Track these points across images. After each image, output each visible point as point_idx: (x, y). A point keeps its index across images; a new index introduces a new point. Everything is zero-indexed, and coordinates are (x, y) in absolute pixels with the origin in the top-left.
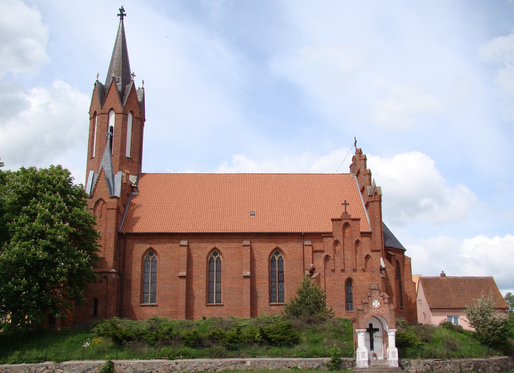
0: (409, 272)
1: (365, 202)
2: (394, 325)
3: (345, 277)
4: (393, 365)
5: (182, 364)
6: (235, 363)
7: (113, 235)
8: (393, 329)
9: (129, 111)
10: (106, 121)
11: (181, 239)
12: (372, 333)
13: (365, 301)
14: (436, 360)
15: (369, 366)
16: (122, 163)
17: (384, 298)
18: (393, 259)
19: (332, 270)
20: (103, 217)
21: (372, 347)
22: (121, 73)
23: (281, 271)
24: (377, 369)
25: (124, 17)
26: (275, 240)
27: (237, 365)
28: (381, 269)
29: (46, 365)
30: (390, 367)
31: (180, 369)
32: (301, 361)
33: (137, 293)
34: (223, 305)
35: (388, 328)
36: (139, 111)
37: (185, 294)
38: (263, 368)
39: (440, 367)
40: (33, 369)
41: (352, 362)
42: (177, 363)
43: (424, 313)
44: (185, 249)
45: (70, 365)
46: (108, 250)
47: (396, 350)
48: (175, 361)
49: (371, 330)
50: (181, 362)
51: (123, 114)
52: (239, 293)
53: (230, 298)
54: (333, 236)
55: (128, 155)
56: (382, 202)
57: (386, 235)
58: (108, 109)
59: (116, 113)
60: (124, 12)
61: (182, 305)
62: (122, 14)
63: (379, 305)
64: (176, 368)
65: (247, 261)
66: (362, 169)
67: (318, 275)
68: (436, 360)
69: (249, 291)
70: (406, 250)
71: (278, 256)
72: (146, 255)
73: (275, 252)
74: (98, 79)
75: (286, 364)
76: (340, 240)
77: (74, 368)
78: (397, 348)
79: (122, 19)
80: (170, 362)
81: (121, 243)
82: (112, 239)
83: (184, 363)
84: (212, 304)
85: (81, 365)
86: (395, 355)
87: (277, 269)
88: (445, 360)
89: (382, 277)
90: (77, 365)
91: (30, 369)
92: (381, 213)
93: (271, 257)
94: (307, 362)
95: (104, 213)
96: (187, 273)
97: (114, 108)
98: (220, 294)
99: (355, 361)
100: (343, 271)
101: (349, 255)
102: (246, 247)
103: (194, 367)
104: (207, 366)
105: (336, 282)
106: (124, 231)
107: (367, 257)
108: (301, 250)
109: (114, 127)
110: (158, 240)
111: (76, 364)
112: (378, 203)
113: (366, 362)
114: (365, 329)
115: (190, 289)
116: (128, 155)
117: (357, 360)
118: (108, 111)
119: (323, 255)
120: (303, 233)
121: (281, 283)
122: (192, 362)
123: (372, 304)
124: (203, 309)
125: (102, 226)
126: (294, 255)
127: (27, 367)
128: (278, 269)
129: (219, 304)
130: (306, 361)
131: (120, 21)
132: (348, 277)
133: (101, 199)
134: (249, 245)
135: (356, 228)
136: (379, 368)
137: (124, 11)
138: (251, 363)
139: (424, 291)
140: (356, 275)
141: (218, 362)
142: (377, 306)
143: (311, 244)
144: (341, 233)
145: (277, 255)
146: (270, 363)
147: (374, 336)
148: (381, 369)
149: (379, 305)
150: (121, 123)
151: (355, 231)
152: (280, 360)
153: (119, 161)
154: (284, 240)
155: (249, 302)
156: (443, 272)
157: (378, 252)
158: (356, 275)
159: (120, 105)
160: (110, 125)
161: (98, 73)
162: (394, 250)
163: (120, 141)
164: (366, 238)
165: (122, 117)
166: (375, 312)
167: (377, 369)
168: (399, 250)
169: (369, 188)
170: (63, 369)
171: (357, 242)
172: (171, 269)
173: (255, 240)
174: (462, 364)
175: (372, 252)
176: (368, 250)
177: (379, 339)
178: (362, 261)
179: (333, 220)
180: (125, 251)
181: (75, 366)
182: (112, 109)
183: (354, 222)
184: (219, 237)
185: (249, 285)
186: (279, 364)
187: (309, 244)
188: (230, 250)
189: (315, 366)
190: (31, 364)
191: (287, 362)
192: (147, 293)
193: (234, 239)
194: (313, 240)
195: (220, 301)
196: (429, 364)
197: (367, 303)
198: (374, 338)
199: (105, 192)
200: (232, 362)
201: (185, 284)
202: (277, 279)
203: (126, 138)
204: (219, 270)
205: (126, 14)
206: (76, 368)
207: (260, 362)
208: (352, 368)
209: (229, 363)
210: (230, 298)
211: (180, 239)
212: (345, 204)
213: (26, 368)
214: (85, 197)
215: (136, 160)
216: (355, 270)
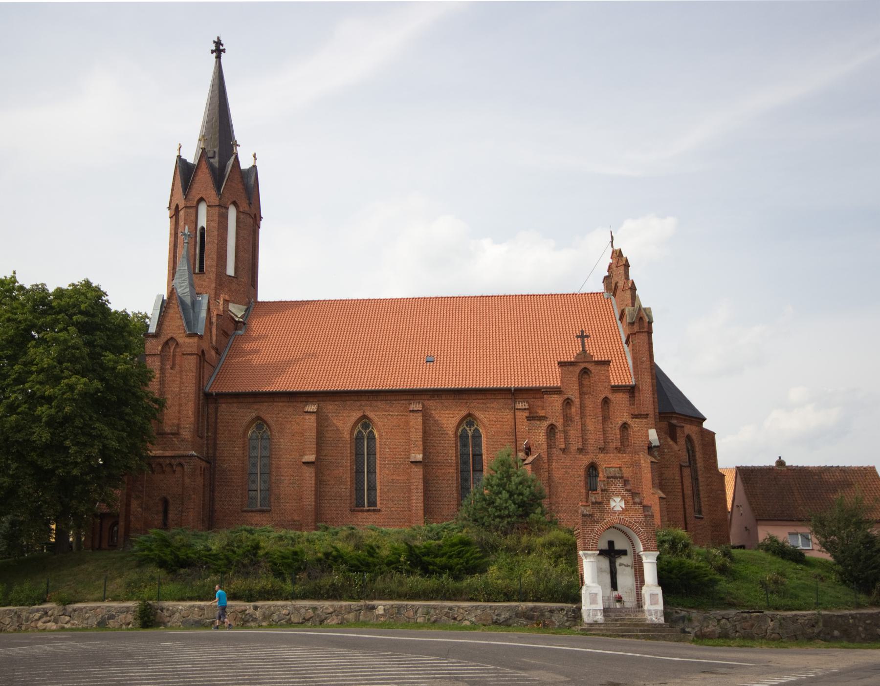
0: (712, 456)
1: (625, 333)
2: (654, 545)
3: (585, 461)
4: (654, 619)
5: (264, 610)
6: (358, 608)
7: (192, 396)
8: (652, 551)
9: (229, 203)
10: (193, 218)
11: (308, 402)
12: (613, 559)
13: (595, 498)
14: (742, 612)
15: (606, 620)
16: (220, 285)
17: (632, 493)
18: (679, 433)
19: (560, 449)
20: (177, 368)
21: (614, 586)
22: (217, 142)
23: (477, 453)
24: (621, 625)
25: (214, 48)
26: (465, 401)
27: (360, 613)
28: (650, 448)
29: (43, 609)
30: (648, 622)
31: (261, 618)
32: (477, 608)
33: (237, 491)
34: (379, 510)
35: (642, 550)
36: (248, 202)
37: (313, 492)
38: (408, 620)
39: (752, 626)
40: (24, 615)
41: (574, 611)
42: (256, 608)
43: (746, 527)
44: (313, 418)
45: (81, 609)
46: (185, 421)
47: (659, 591)
48: (252, 604)
49: (611, 553)
50: (262, 605)
51: (219, 206)
52: (405, 490)
53: (391, 499)
54: (561, 391)
55: (230, 271)
56: (653, 335)
57: (662, 384)
58: (196, 200)
59: (208, 206)
60: (222, 46)
61: (308, 510)
62: (218, 50)
63: (624, 507)
64: (254, 616)
65: (417, 436)
66: (621, 282)
67: (535, 458)
68: (742, 612)
69: (421, 486)
70: (704, 419)
71: (473, 429)
72: (251, 428)
73: (467, 422)
74: (179, 153)
75: (449, 613)
76: (574, 399)
77: (87, 615)
78: (660, 588)
79: (218, 57)
80: (245, 606)
81: (210, 411)
82: (190, 403)
83: (268, 608)
84: (362, 508)
85: (98, 610)
86: (658, 600)
87: (471, 449)
88: (762, 612)
89: (652, 462)
90: (92, 609)
91: (19, 616)
92: (652, 352)
93: (460, 430)
94: (488, 609)
95: (178, 361)
96: (317, 458)
97: (205, 198)
98: (374, 491)
99: (580, 609)
100: (580, 451)
101: (593, 425)
102: (416, 415)
103: (284, 614)
104: (308, 614)
105: (569, 471)
106: (213, 391)
107: (625, 427)
108: (510, 417)
109: (205, 227)
110: (270, 404)
111: (92, 607)
112: (646, 335)
113: (598, 612)
114: (596, 550)
115: (325, 483)
116: (230, 271)
117: (584, 608)
118: (195, 203)
119: (545, 424)
120: (513, 389)
121: (478, 474)
122: (282, 607)
123: (608, 504)
124: (346, 516)
125: (174, 381)
126: (498, 426)
127: (15, 611)
128: (472, 450)
129: (372, 508)
130: (485, 607)
131: (216, 61)
132: (590, 461)
133: (172, 338)
134: (421, 411)
135: (603, 378)
136: (625, 624)
137: (222, 45)
138: (384, 609)
139: (745, 489)
140: (605, 458)
141: (327, 606)
142: (618, 508)
143: (527, 407)
144: (576, 387)
145: (470, 427)
146: (420, 610)
147: (617, 564)
148: (629, 626)
149: (624, 507)
150: (217, 222)
151: (601, 382)
152: (438, 605)
153: (214, 282)
154: (481, 401)
155: (421, 505)
156: (780, 458)
157: (644, 418)
158: (605, 458)
159: (214, 192)
160: (199, 227)
161: (180, 144)
162: (681, 418)
163: (215, 250)
164: (621, 394)
165: (217, 211)
166: (615, 519)
167: (621, 625)
168: (692, 419)
169: (629, 311)
170: (70, 616)
171: (606, 401)
172: (291, 451)
173: (432, 401)
174: (799, 621)
175: (632, 418)
176: (625, 414)
177: (629, 569)
178: (616, 434)
179: (561, 364)
180: (216, 423)
181: (89, 612)
182: (201, 200)
183: (599, 367)
184: (371, 398)
185: (421, 476)
186: (435, 612)
187: (524, 407)
188: (389, 420)
189: (503, 616)
190: (22, 607)
191: (451, 608)
192: (254, 491)
193: (396, 400)
194: (532, 400)
195: (375, 504)
196: (728, 619)
197: (600, 503)
198: (618, 567)
199: (178, 327)
200: (352, 607)
201: (313, 475)
202: (471, 467)
203: (227, 245)
204: (372, 453)
205: (224, 49)
206: (90, 615)
207: (402, 609)
208: (573, 623)
209: (346, 609)
210: (391, 499)
211: (306, 402)
212: (583, 336)
213: (13, 614)
214: (147, 335)
215: (244, 279)
216: (602, 450)
